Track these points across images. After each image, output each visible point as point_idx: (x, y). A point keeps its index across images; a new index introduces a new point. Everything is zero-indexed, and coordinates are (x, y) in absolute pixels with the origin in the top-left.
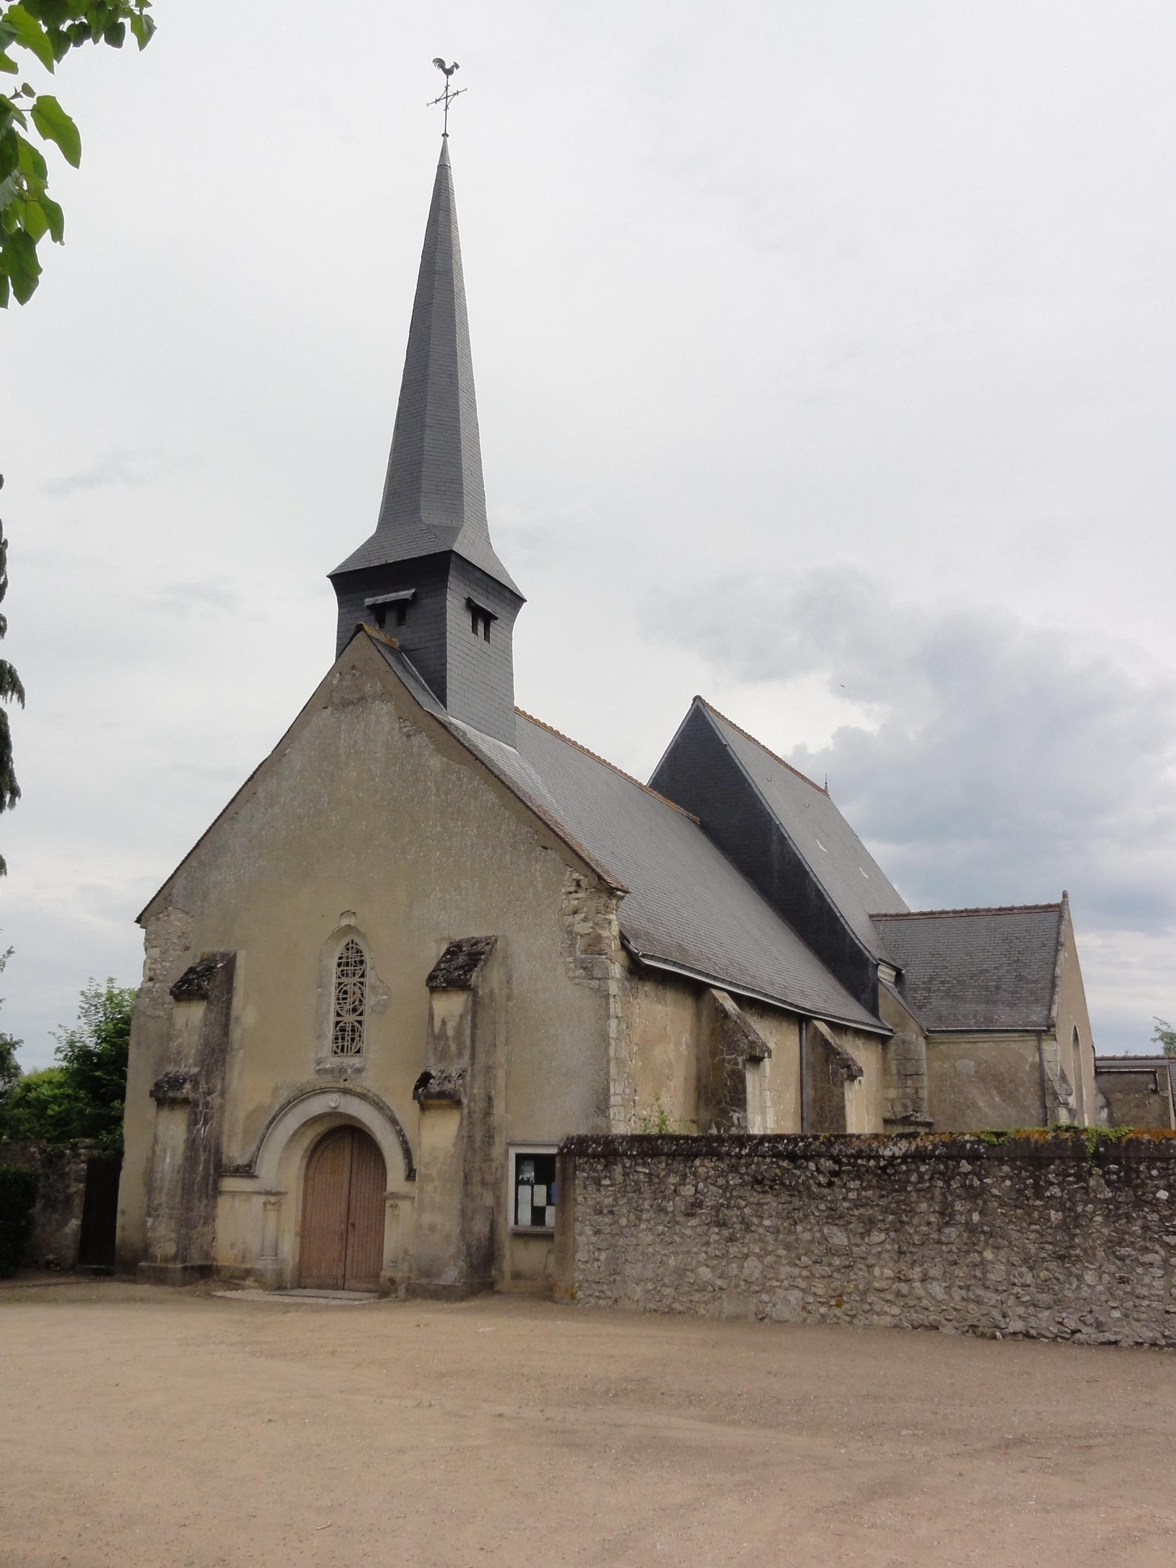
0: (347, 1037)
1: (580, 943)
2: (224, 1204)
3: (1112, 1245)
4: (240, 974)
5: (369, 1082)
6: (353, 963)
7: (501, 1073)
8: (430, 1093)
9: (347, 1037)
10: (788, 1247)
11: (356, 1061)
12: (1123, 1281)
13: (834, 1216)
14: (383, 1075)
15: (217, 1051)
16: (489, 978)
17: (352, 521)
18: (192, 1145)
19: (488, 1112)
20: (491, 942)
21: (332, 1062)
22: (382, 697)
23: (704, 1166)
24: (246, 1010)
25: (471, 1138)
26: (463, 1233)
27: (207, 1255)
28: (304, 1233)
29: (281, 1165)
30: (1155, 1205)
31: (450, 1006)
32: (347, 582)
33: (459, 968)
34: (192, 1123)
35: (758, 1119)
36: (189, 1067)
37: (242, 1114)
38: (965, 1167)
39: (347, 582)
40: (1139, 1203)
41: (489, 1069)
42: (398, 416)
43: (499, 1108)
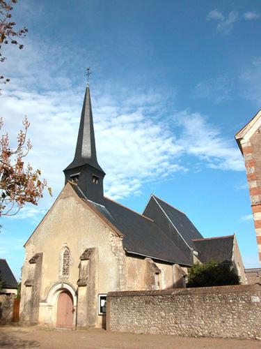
0: (66, 271)
1: (113, 248)
2: (40, 308)
3: (220, 314)
4: (44, 258)
5: (70, 281)
6: (67, 254)
7: (97, 278)
8: (81, 284)
9: (66, 271)
10: (153, 316)
11: (67, 276)
12: (223, 322)
13: (162, 309)
14: (73, 278)
15: (38, 273)
16: (94, 257)
17: (68, 159)
18: (33, 295)
19: (94, 287)
20: (94, 249)
21: (62, 276)
22: (72, 196)
23: (135, 298)
24: (45, 265)
25: (90, 293)
26: (88, 315)
27: (37, 320)
28: (58, 315)
29: (53, 299)
30: (230, 303)
31: (85, 263)
32: (65, 171)
33: (87, 255)
34: (33, 290)
35: (240, 166)
36: (32, 278)
37: (44, 289)
38: (189, 296)
39: (65, 171)
40: (226, 303)
41: (94, 277)
42: (130, 210)
43: (96, 286)
